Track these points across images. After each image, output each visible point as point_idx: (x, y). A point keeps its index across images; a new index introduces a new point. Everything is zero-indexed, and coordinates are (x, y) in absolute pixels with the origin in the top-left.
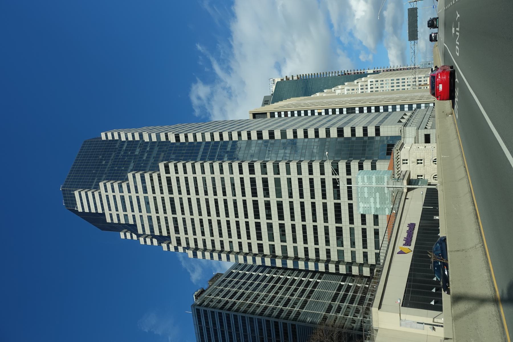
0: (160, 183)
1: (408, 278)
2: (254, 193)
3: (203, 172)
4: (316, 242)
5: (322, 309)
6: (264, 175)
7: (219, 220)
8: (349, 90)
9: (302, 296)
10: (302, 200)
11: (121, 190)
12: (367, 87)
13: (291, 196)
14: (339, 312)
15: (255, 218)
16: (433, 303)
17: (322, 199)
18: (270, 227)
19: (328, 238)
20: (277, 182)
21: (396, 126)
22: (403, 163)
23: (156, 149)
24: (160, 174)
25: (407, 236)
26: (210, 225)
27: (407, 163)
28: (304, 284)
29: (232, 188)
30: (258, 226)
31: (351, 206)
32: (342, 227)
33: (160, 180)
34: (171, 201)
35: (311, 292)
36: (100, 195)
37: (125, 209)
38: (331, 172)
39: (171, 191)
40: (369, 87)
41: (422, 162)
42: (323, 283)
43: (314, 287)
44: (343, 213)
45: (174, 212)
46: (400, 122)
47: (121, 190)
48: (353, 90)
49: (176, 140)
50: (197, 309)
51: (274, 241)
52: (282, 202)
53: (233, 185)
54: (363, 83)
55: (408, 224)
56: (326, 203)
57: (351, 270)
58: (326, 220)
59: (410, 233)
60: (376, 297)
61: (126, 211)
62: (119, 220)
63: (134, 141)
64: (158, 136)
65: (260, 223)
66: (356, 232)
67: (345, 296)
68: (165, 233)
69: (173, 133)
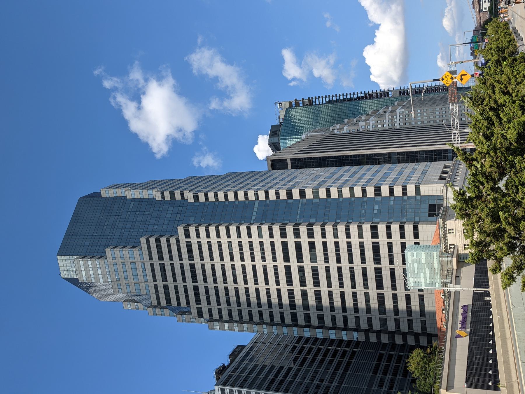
1: (468, 362)
3: (229, 236)
16: (490, 384)
17: (361, 264)
18: (298, 246)
19: (369, 305)
21: (437, 185)
22: (450, 233)
24: (179, 239)
25: (462, 319)
26: (236, 293)
27: (453, 233)
28: (339, 354)
29: (262, 253)
30: (285, 246)
35: (349, 364)
38: (403, 280)
42: (361, 353)
43: (352, 357)
46: (441, 178)
50: (221, 389)
51: (309, 310)
53: (210, 249)
55: (462, 306)
57: (394, 339)
58: (366, 286)
59: (465, 315)
60: (443, 380)
66: (399, 298)
67: (387, 368)
68: (183, 303)
69: (190, 191)
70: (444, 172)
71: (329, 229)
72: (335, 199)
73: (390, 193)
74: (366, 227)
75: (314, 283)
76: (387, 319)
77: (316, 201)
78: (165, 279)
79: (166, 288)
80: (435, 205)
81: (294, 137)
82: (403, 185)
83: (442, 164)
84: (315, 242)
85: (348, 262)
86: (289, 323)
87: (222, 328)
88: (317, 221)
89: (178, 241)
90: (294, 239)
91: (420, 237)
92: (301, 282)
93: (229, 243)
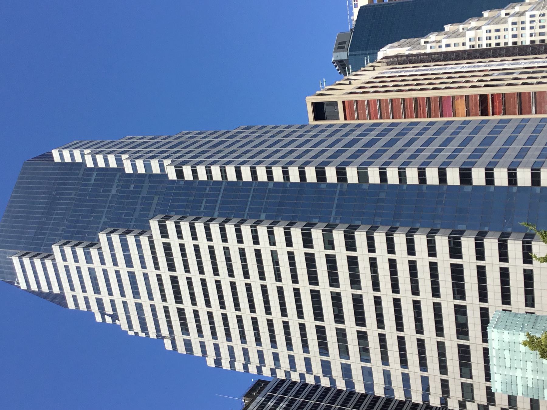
0: (154, 253)
3: (273, 243)
4: (419, 329)
6: (330, 249)
7: (241, 248)
8: (490, 31)
11: (89, 259)
12: (523, 26)
18: (331, 261)
20: (353, 263)
23: (146, 185)
24: (152, 237)
26: (240, 324)
30: (310, 260)
33: (152, 247)
34: (172, 281)
36: (55, 265)
37: (97, 290)
39: (171, 266)
40: (528, 25)
44: (466, 276)
45: (178, 299)
47: (89, 259)
48: (498, 30)
49: (178, 176)
52: (361, 296)
54: (515, 19)
56: (439, 304)
61: (99, 293)
63: (107, 170)
64: (147, 166)
65: (313, 254)
71: (380, 238)
72: (501, 188)
73: (381, 179)
74: (200, 226)
75: (356, 319)
76: (474, 386)
77: (271, 185)
82: (535, 167)
84: (358, 257)
85: (410, 293)
88: (471, 227)
89: (151, 242)
91: (486, 258)
92: (335, 316)
93: (226, 249)
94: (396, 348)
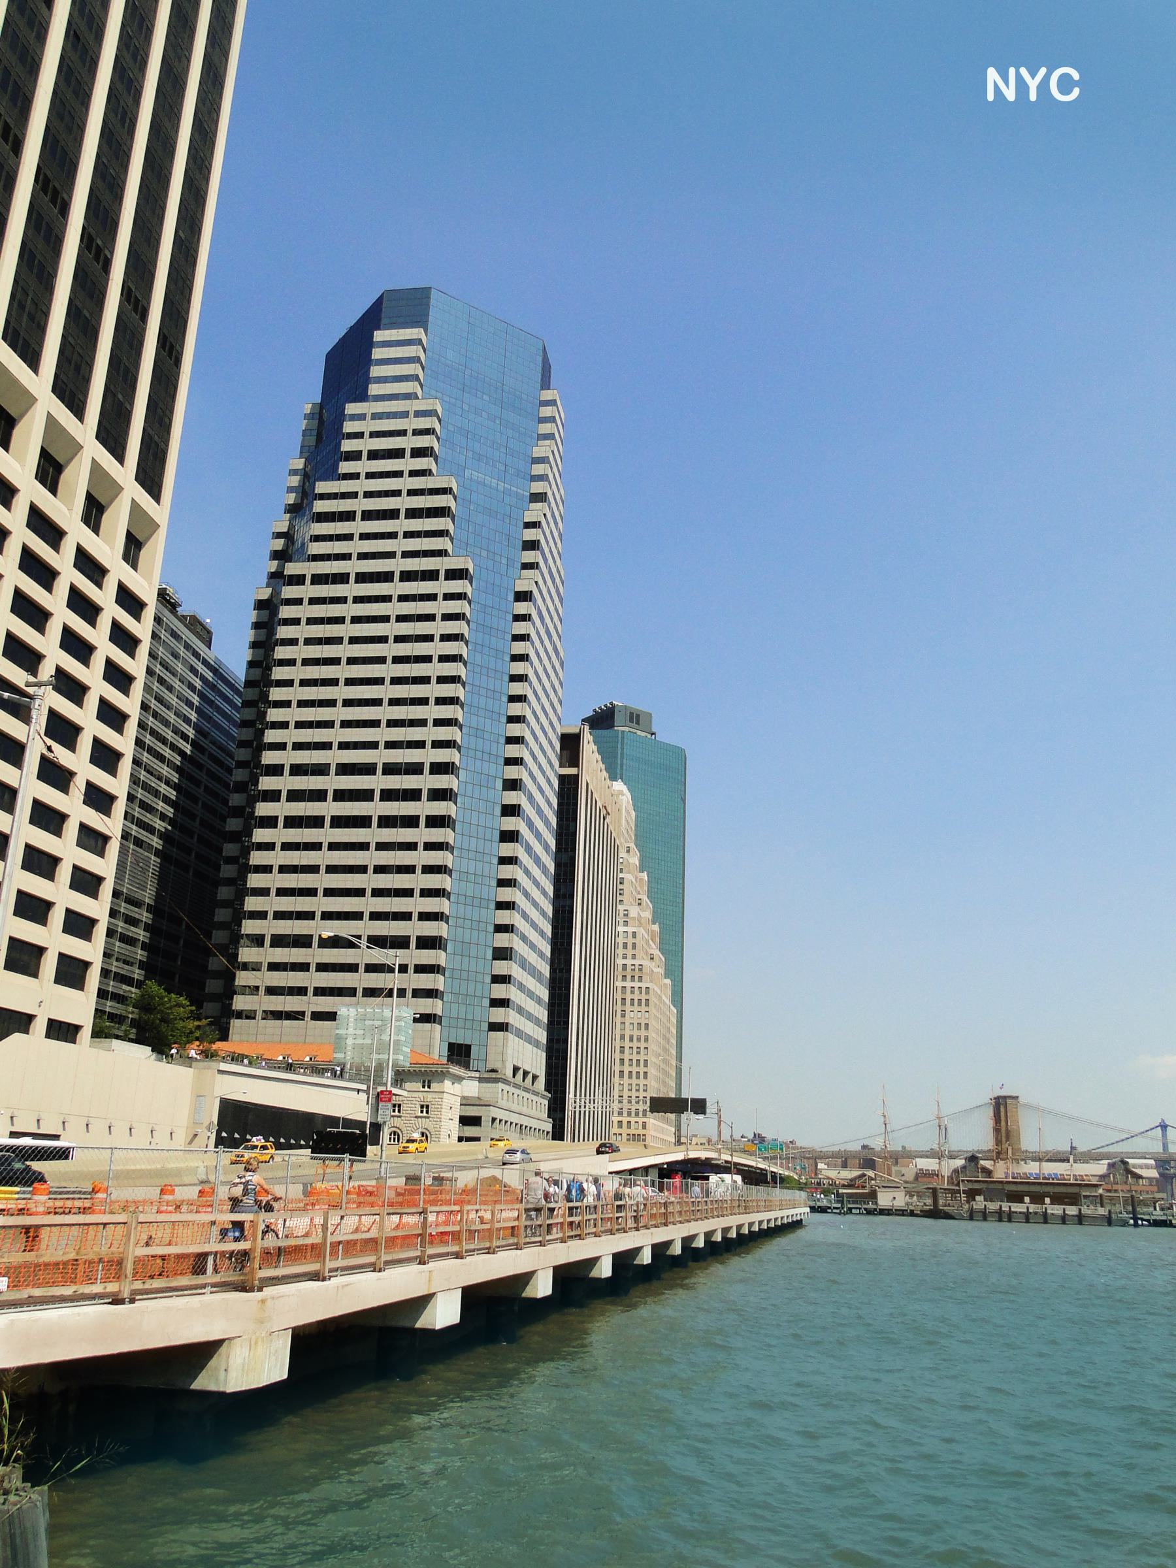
2: (391, 769)
5: (133, 886)
9: (180, 699)
10: (362, 968)
13: (381, 846)
14: (126, 923)
15: (335, 791)
31: (351, 992)
32: (354, 520)
41: (425, 1114)
62: (354, 418)
68: (320, 506)
70: (525, 1073)
78: (368, 515)
79: (348, 516)
80: (468, 1054)
81: (619, 751)
83: (541, 1072)
86: (314, 508)
87: (290, 490)
90: (431, 739)
94: (288, 1008)
